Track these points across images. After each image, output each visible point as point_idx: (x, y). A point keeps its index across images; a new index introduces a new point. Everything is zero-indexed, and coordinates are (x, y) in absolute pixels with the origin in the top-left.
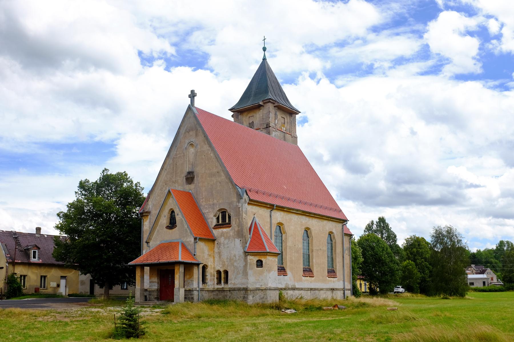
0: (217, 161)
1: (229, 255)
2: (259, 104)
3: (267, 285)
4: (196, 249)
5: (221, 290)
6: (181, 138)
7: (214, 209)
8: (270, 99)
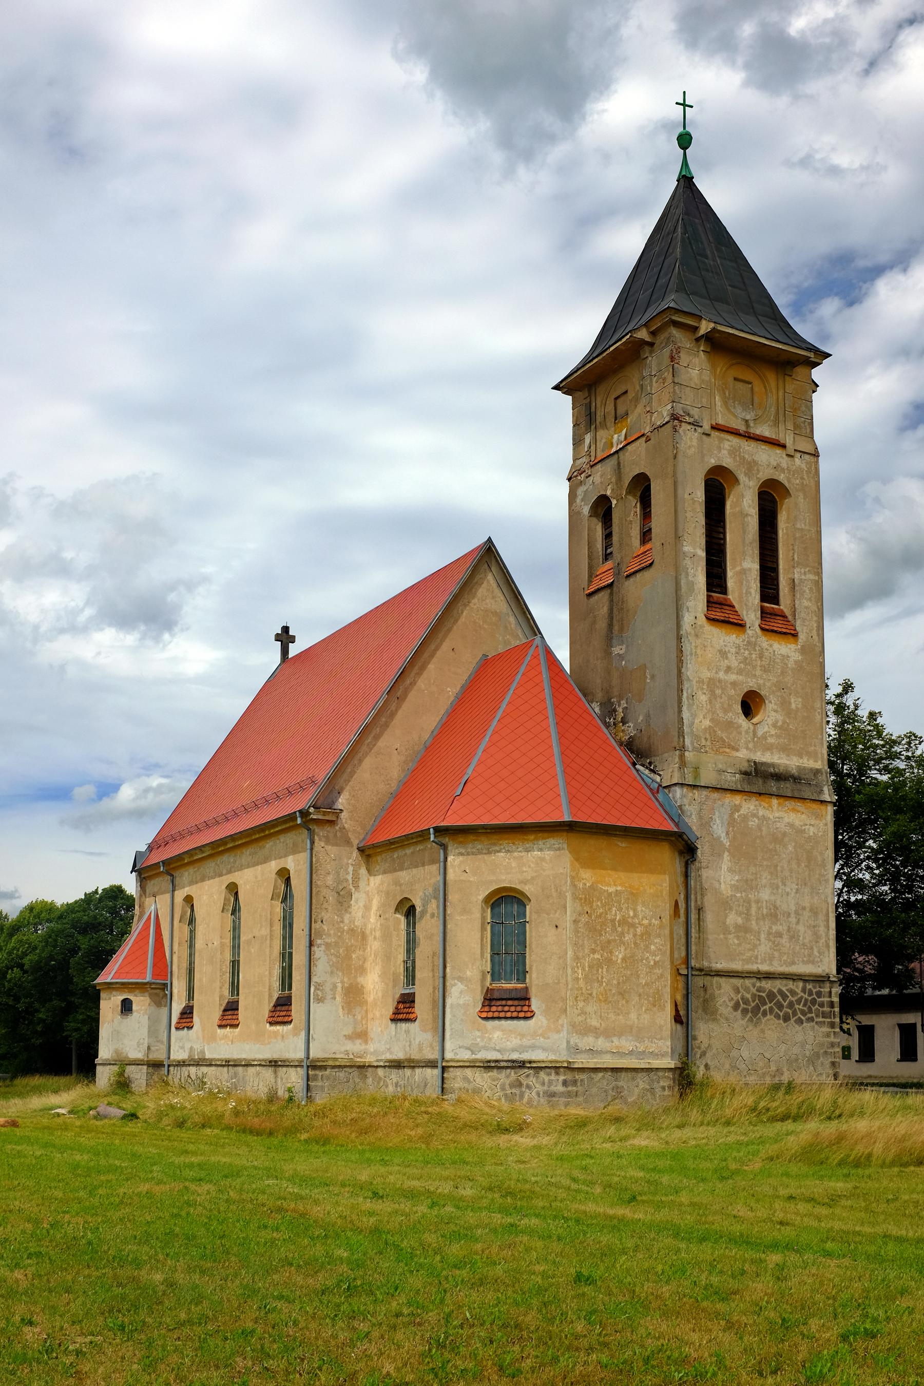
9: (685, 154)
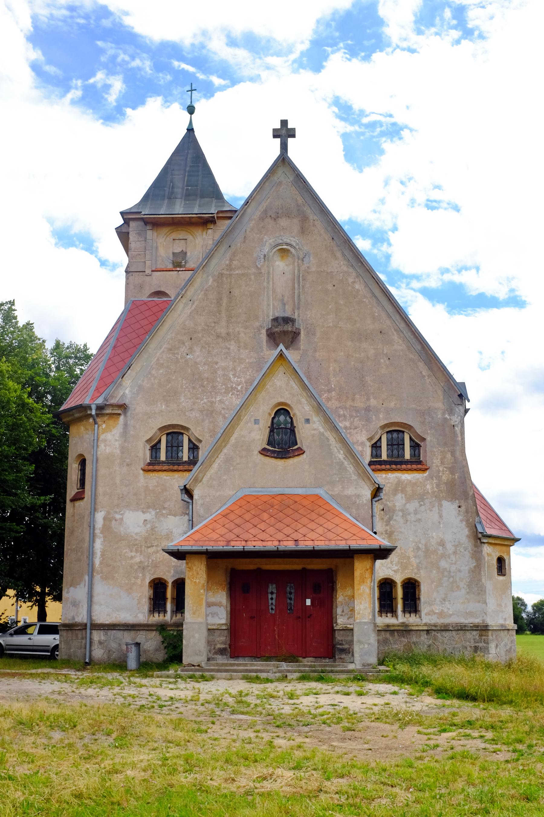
1: (423, 542)
7: (368, 420)
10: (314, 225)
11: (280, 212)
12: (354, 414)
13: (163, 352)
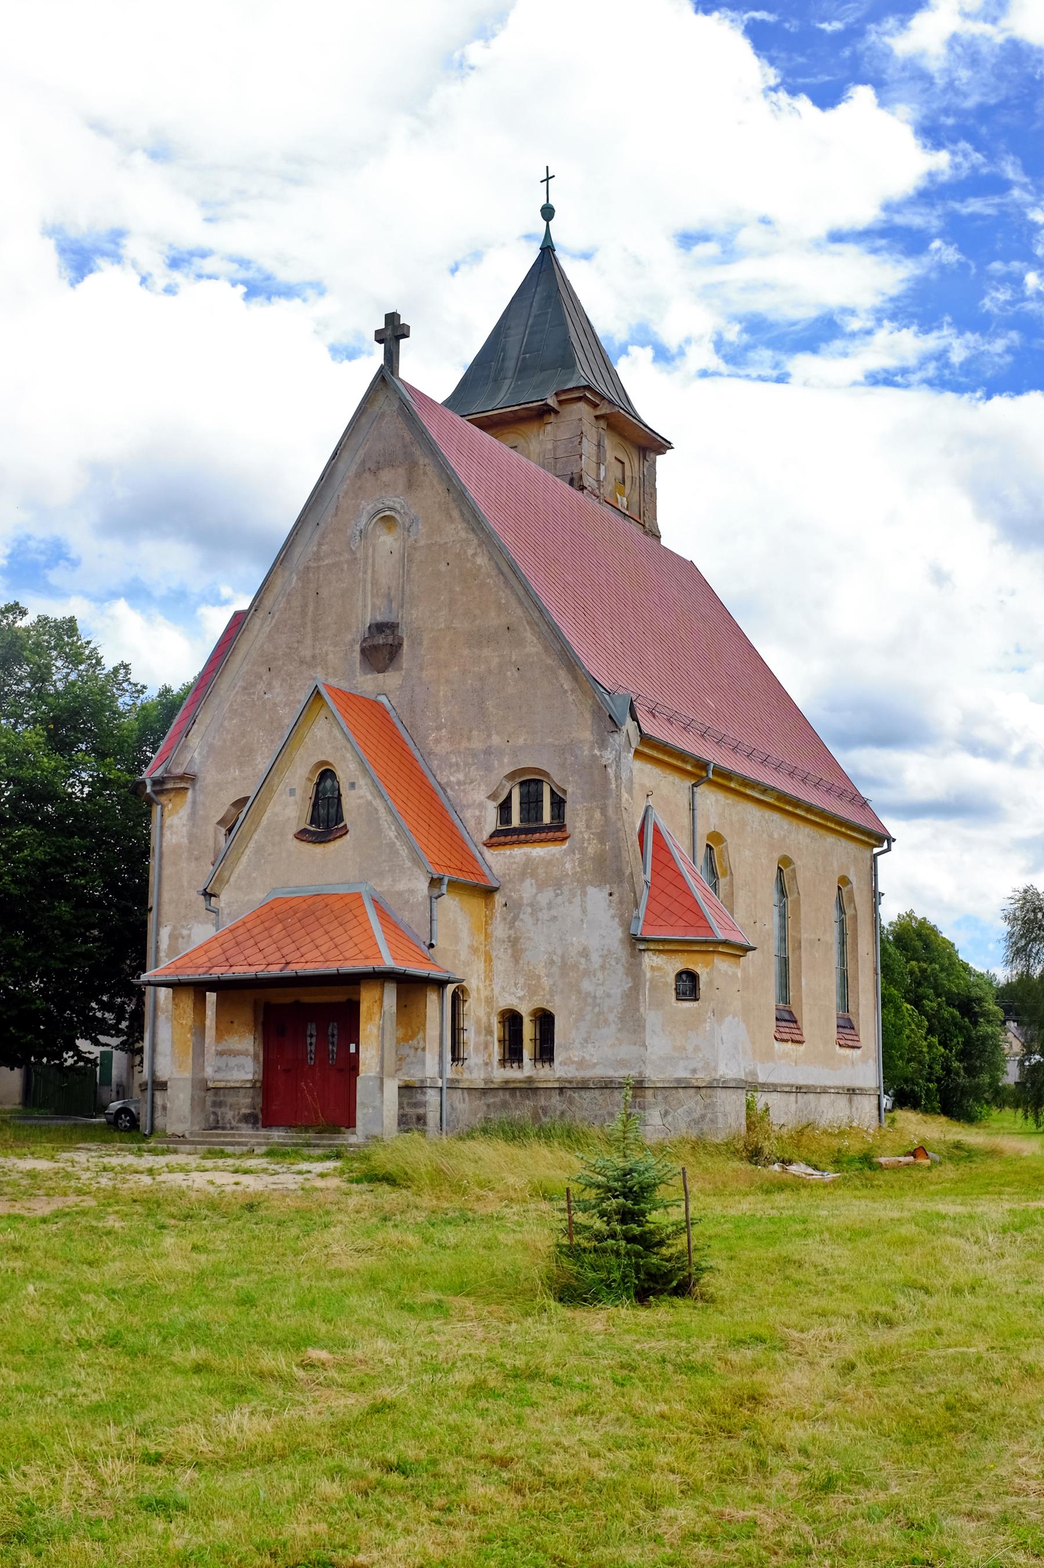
0: (502, 586)
1: (559, 952)
2: (546, 405)
3: (715, 1069)
4: (435, 923)
5: (520, 1089)
6: (342, 495)
7: (488, 769)
8: (588, 388)
9: (548, 225)
10: (425, 473)
11: (382, 460)
12: (470, 760)
13: (237, 692)
